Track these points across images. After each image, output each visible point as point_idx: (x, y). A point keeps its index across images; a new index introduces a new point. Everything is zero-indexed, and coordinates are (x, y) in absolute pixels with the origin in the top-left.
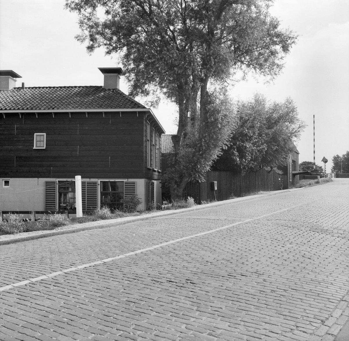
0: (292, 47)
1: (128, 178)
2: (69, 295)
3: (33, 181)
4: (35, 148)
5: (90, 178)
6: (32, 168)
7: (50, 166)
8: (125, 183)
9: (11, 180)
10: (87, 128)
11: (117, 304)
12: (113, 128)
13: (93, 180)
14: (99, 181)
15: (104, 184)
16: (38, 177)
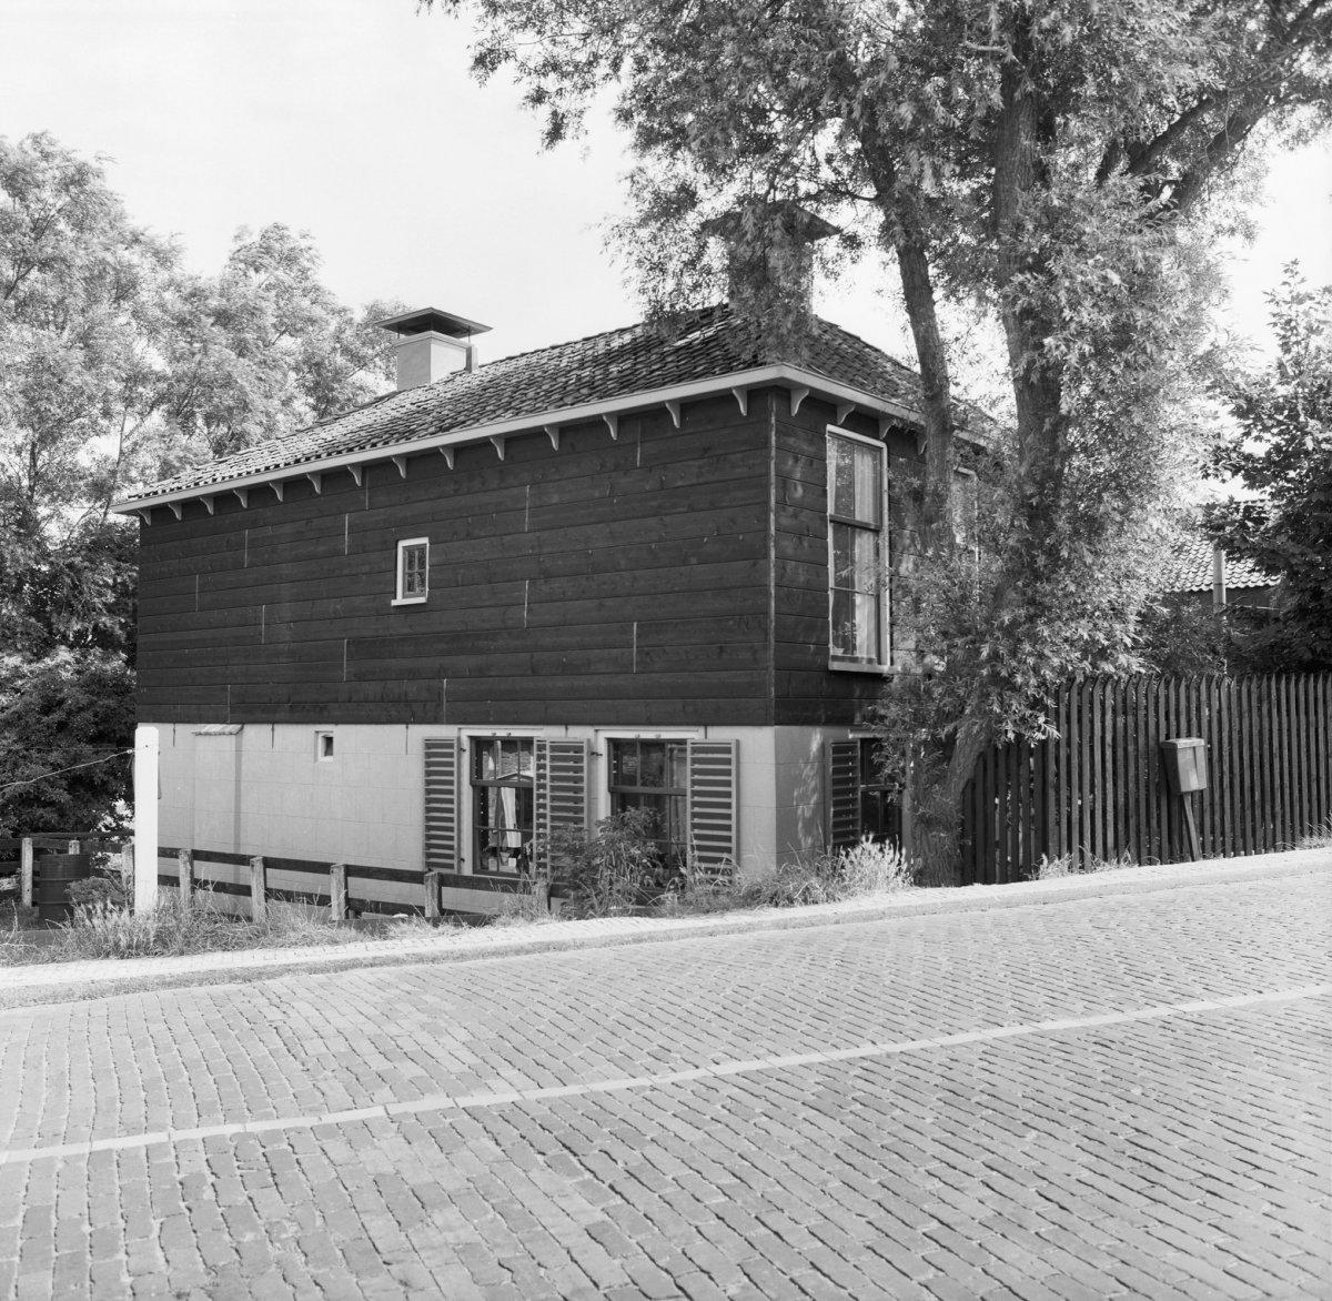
0: (111, 159)
1: (705, 722)
2: (1057, 1071)
3: (396, 732)
4: (399, 601)
5: (566, 723)
6: (390, 684)
7: (439, 674)
8: (694, 750)
9: (342, 733)
10: (555, 499)
11: (730, 1186)
12: (648, 488)
13: (578, 734)
14: (599, 738)
15: (615, 744)
16: (407, 722)
